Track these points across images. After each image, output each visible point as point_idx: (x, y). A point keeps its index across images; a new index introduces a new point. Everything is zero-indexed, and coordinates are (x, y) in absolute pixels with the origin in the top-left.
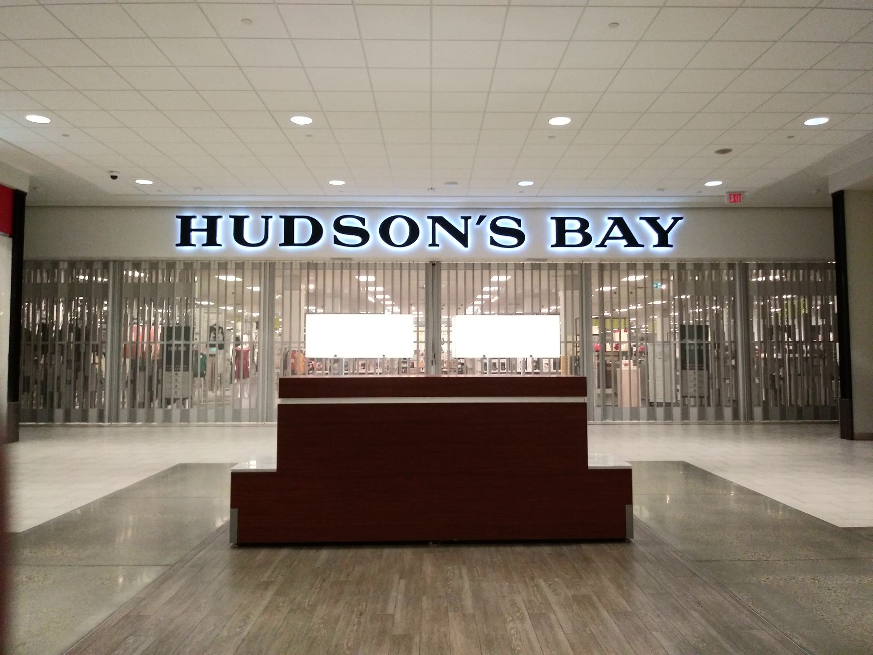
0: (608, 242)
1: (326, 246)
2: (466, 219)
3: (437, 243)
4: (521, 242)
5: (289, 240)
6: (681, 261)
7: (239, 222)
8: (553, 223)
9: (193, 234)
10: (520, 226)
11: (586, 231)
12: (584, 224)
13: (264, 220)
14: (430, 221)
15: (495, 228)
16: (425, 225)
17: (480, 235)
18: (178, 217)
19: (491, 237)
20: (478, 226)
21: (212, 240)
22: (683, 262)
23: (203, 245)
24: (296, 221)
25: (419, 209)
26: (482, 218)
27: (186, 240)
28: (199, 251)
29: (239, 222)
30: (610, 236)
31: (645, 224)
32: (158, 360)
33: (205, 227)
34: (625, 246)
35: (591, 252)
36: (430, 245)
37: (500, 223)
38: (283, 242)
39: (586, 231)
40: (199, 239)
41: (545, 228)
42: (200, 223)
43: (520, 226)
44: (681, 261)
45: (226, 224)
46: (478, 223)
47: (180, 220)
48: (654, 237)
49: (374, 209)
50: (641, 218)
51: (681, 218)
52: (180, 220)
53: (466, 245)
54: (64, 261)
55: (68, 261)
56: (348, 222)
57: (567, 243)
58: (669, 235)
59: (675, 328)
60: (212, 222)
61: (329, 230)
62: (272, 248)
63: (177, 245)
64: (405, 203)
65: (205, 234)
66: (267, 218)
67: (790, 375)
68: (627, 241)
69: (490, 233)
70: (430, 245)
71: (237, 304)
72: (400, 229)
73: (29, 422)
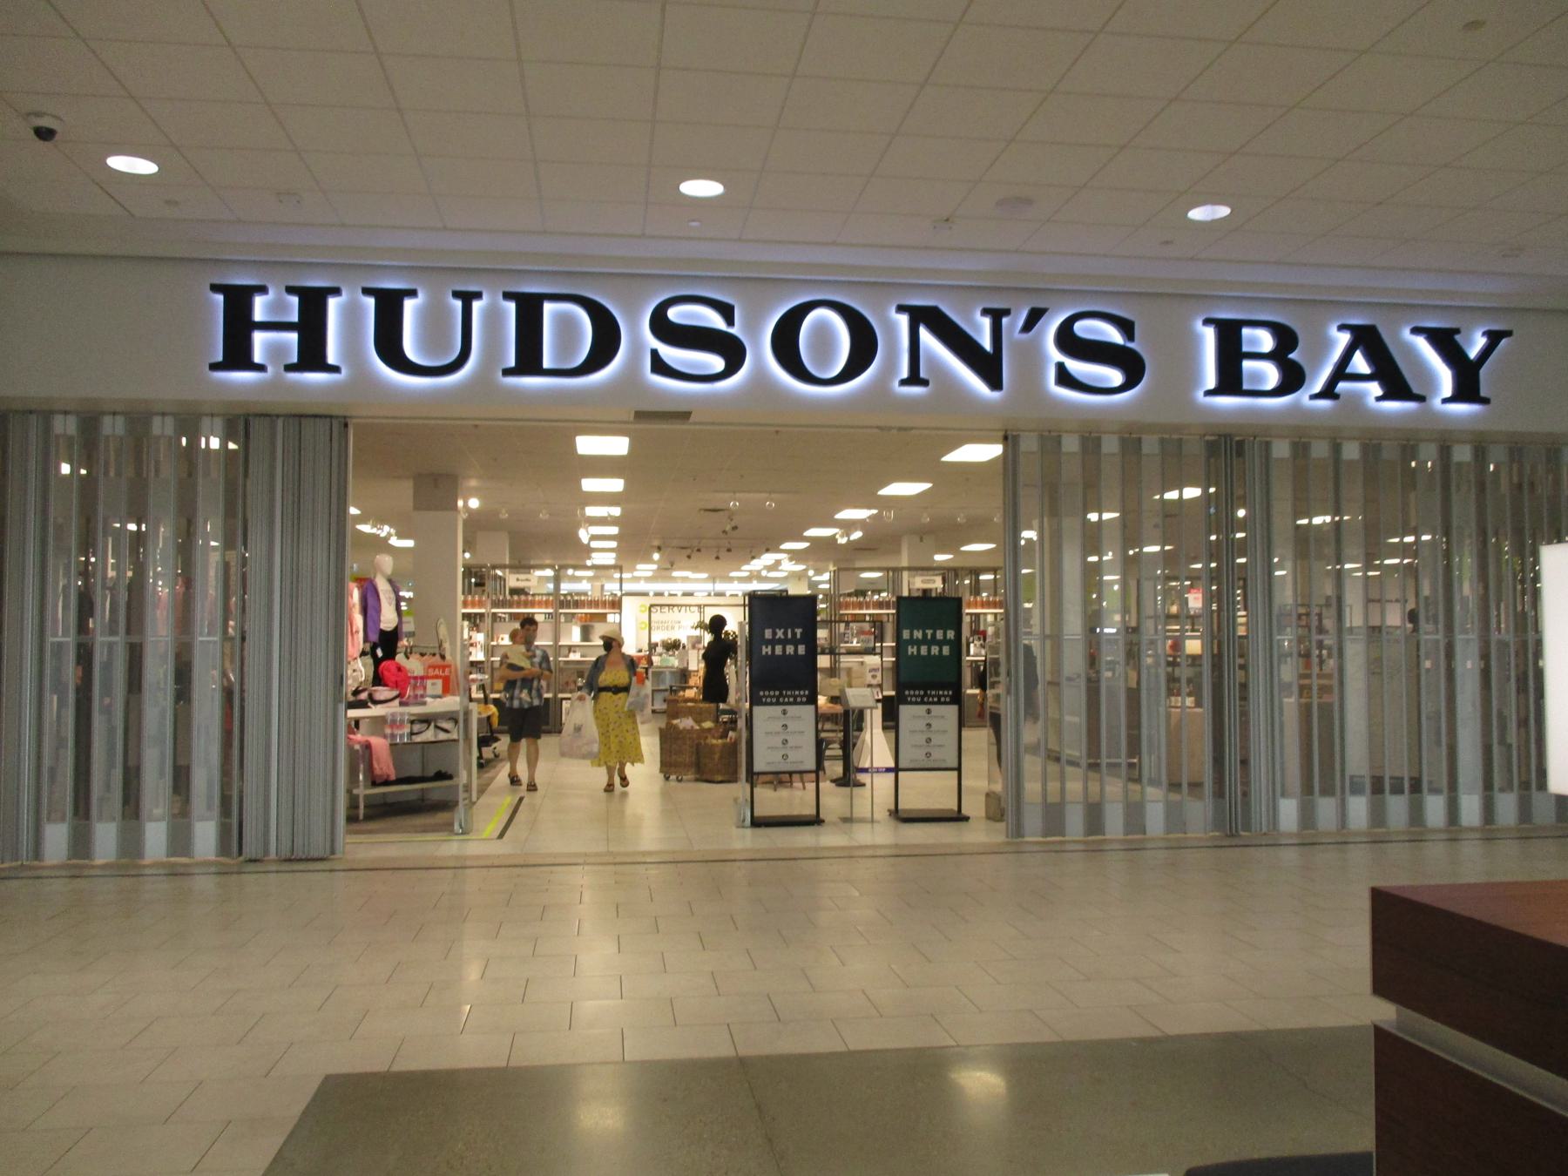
0: (1342, 386)
1: (631, 372)
2: (997, 315)
3: (922, 375)
4: (732, 367)
5: (529, 361)
6: (1370, 440)
7: (389, 307)
8: (1209, 335)
9: (259, 338)
10: (730, 322)
11: (1291, 356)
12: (1286, 339)
13: (458, 304)
14: (903, 320)
15: (1068, 341)
16: (891, 329)
17: (1034, 356)
18: (215, 288)
19: (1061, 368)
20: (1025, 336)
21: (312, 356)
22: (1375, 442)
23: (290, 368)
24: (548, 308)
25: (879, 288)
26: (1035, 316)
27: (238, 355)
28: (275, 384)
29: (389, 307)
30: (1348, 370)
31: (1422, 345)
32: (115, 768)
33: (295, 318)
34: (1379, 399)
35: (1296, 408)
36: (904, 382)
37: (1083, 328)
38: (220, 358)
39: (1291, 356)
40: (275, 350)
41: (1191, 346)
42: (277, 306)
43: (730, 322)
44: (1300, 438)
45: (352, 316)
46: (1028, 326)
47: (220, 298)
48: (1445, 379)
49: (765, 283)
50: (1416, 331)
51: (1508, 334)
52: (220, 298)
53: (995, 382)
54: (164, 414)
55: (77, 413)
56: (685, 315)
57: (1245, 387)
58: (1483, 372)
59: (934, 641)
60: (313, 303)
61: (637, 335)
62: (481, 379)
63: (215, 367)
64: (936, 272)
65: (293, 337)
66: (467, 298)
67: (29, 770)
68: (1382, 385)
69: (1055, 355)
70: (904, 382)
71: (1373, 601)
72: (823, 335)
73: (1372, 1168)
